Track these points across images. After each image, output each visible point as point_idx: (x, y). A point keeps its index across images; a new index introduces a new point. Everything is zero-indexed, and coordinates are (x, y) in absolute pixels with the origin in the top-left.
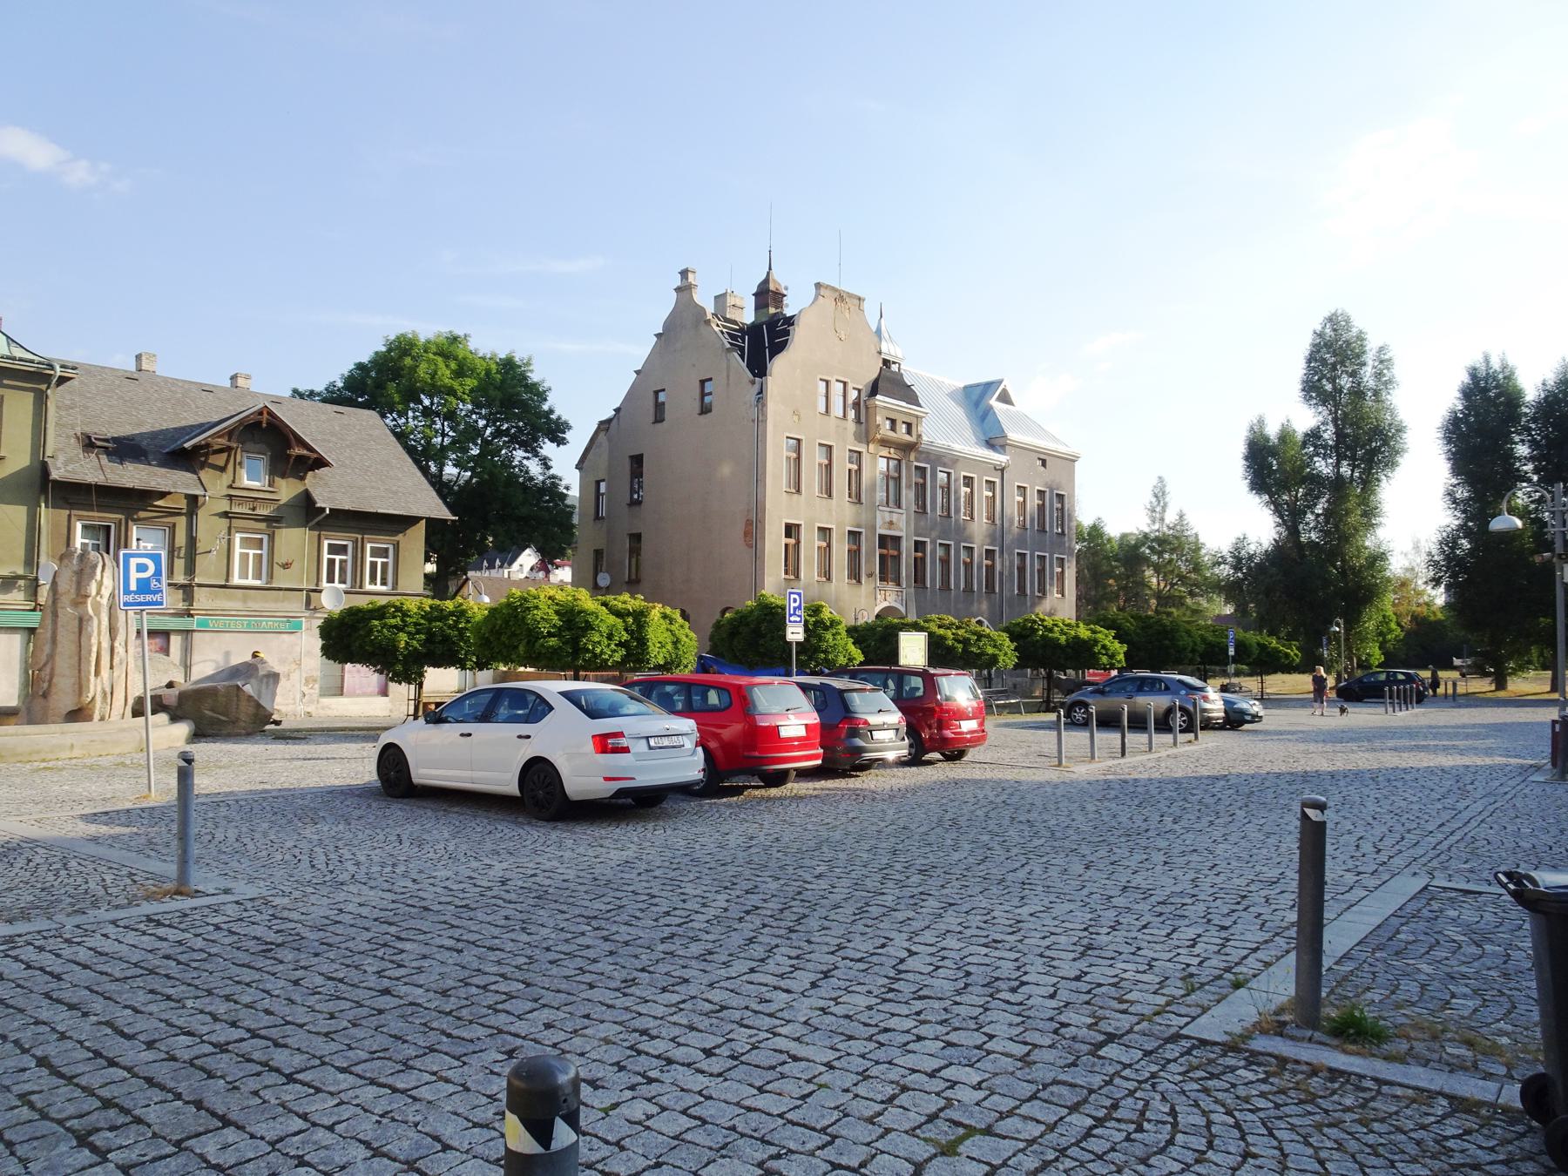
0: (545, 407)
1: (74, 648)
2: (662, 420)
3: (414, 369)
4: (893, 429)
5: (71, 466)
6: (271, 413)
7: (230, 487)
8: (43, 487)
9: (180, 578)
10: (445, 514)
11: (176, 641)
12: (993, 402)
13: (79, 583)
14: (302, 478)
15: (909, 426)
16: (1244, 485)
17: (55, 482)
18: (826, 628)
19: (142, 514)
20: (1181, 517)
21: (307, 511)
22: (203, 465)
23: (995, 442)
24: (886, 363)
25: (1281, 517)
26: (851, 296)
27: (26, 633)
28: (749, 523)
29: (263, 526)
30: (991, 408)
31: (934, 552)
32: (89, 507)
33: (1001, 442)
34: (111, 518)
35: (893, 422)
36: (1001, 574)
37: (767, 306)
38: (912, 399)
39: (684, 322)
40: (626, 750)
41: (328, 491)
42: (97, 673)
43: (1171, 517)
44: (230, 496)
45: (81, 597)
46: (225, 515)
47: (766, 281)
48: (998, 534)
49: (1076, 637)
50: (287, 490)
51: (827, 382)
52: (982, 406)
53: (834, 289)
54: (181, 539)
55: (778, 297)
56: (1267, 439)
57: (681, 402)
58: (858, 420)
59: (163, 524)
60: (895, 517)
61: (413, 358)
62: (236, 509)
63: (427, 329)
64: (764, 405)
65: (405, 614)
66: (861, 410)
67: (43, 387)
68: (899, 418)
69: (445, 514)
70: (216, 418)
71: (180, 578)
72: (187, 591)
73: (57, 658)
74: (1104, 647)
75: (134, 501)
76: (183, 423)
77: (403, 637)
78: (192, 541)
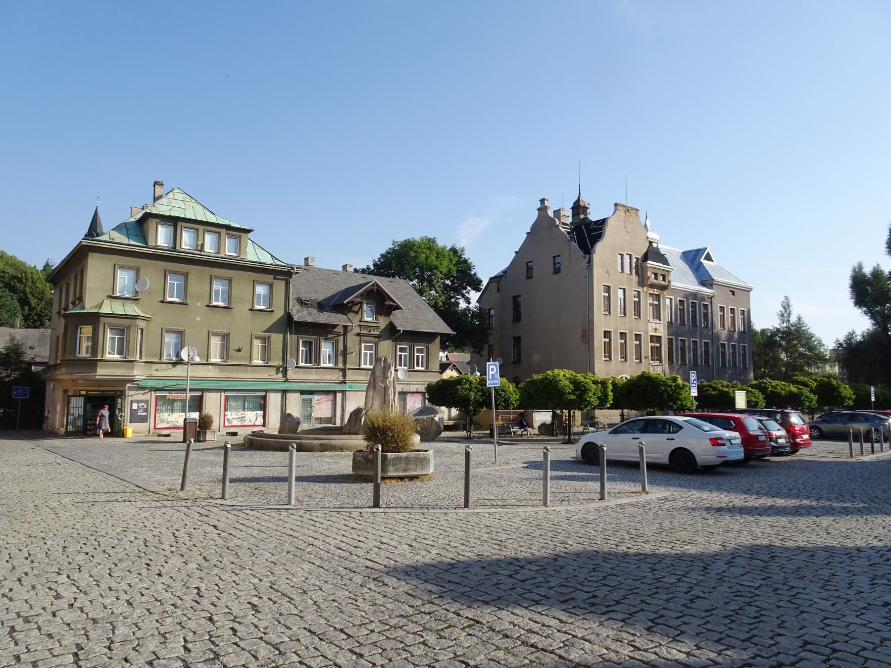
0: (473, 273)
2: (531, 277)
3: (416, 257)
4: (656, 278)
5: (300, 315)
6: (378, 285)
8: (288, 324)
9: (341, 366)
10: (448, 330)
11: (339, 396)
12: (702, 260)
15: (664, 276)
16: (851, 303)
18: (681, 389)
20: (799, 319)
21: (392, 332)
23: (706, 280)
24: (651, 243)
25: (875, 320)
26: (632, 209)
28: (584, 331)
29: (372, 339)
30: (701, 263)
31: (689, 345)
33: (710, 282)
34: (312, 338)
35: (656, 275)
36: (712, 355)
37: (579, 214)
38: (664, 261)
39: (544, 224)
40: (724, 445)
41: (402, 321)
43: (793, 319)
45: (385, 377)
46: (358, 334)
47: (577, 202)
48: (730, 338)
49: (790, 392)
50: (383, 322)
51: (622, 255)
52: (696, 263)
53: (624, 206)
54: (341, 348)
55: (585, 209)
56: (864, 275)
57: (543, 267)
58: (637, 273)
60: (658, 326)
61: (415, 252)
63: (416, 235)
64: (592, 269)
65: (471, 383)
66: (640, 269)
68: (659, 272)
69: (448, 330)
71: (341, 366)
72: (344, 371)
74: (806, 397)
75: (324, 330)
77: (473, 394)
78: (345, 347)
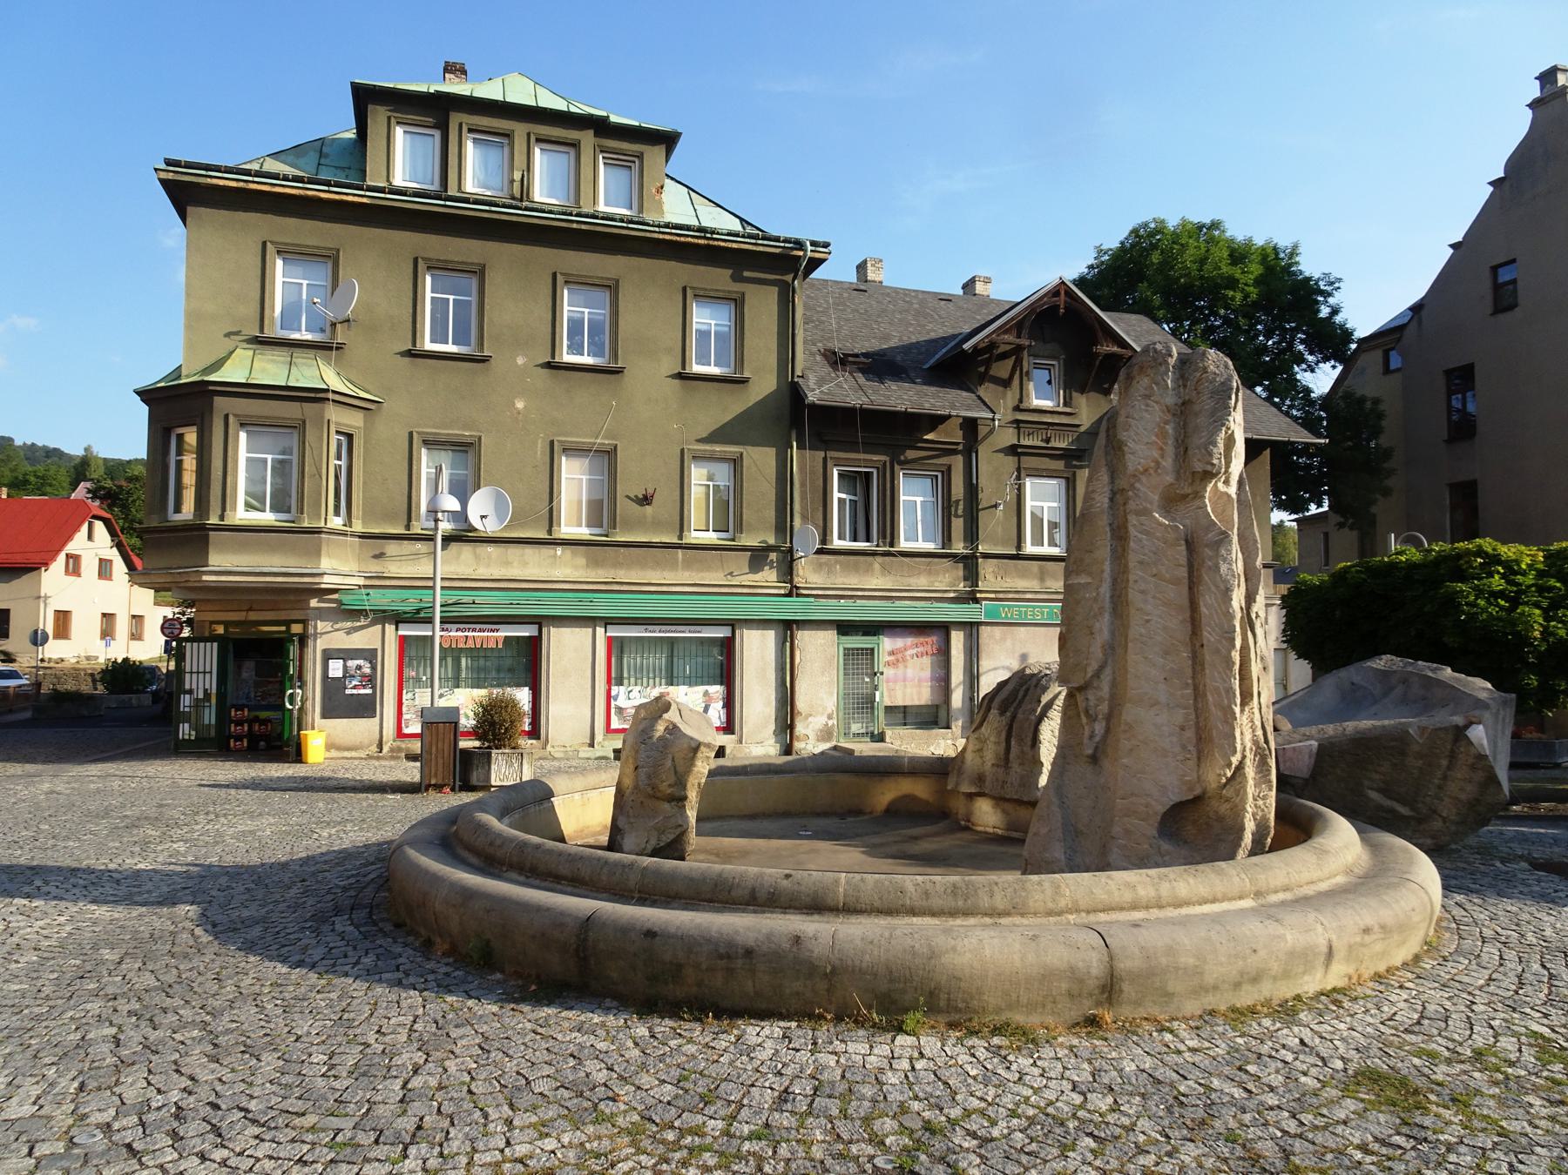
1: (1178, 624)
2: (1512, 307)
5: (822, 387)
7: (1017, 409)
11: (957, 639)
13: (1183, 450)
14: (1107, 392)
17: (813, 406)
19: (911, 454)
22: (983, 378)
27: (781, 627)
29: (1060, 465)
32: (852, 446)
34: (868, 461)
42: (1246, 697)
44: (1017, 422)
46: (1013, 450)
59: (936, 468)
62: (1026, 442)
67: (789, 278)
70: (967, 329)
71: (959, 547)
72: (970, 565)
73: (1133, 657)
75: (896, 435)
76: (933, 335)
78: (972, 490)
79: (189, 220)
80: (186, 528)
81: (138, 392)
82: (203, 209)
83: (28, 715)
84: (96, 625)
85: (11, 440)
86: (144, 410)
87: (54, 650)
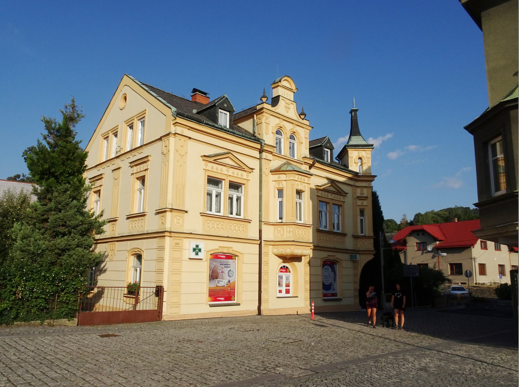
79: (483, 27)
80: (502, 198)
81: (466, 128)
82: (491, 9)
83: (463, 307)
84: (497, 269)
85: (469, 208)
86: (470, 138)
87: (480, 279)
